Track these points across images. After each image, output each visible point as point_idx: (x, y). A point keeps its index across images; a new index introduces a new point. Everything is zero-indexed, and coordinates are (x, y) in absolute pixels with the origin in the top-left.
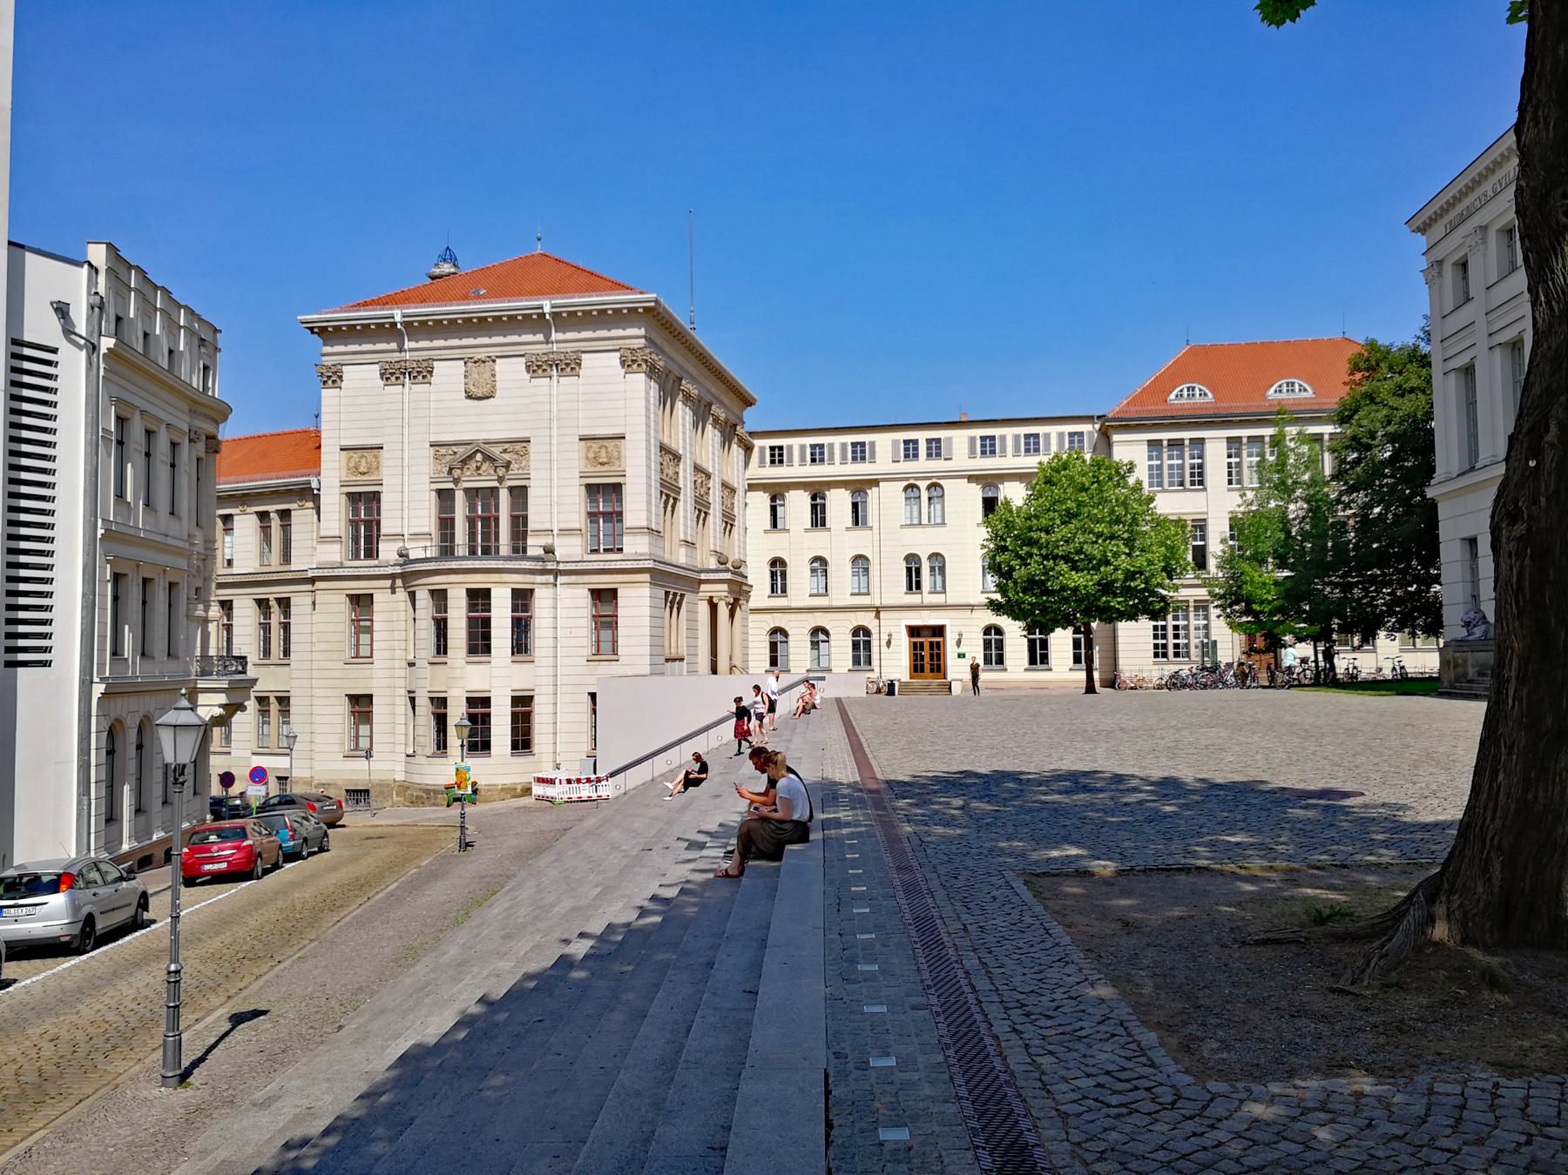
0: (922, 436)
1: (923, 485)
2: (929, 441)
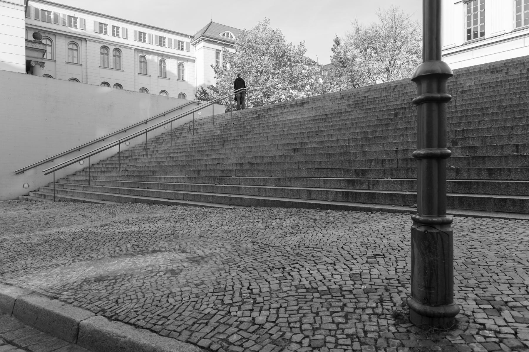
1: (111, 48)
2: (113, 27)
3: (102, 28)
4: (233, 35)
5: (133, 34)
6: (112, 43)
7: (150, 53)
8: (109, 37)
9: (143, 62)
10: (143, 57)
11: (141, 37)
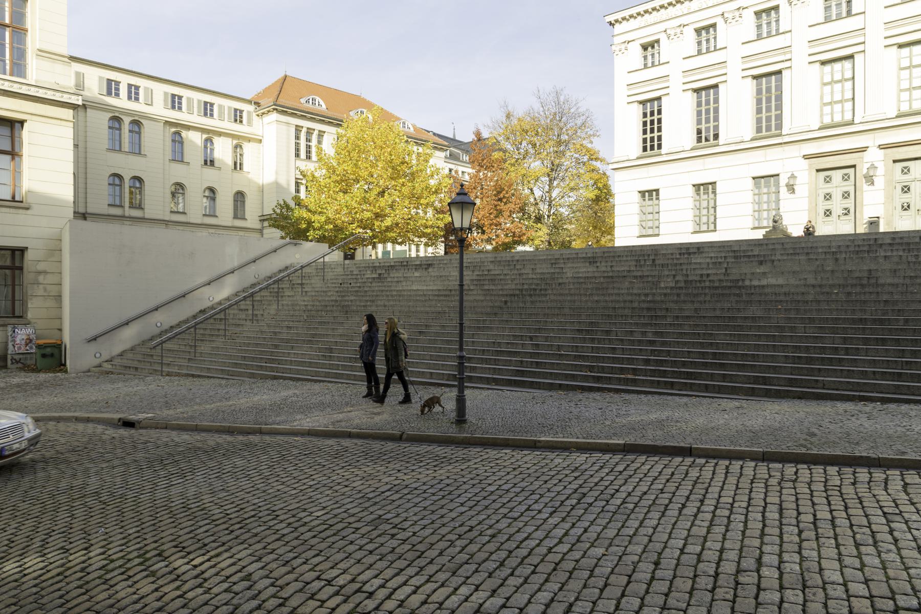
0: (125, 80)
3: (112, 88)
4: (322, 103)
5: (162, 97)
6: (128, 113)
7: (188, 128)
8: (122, 102)
9: (178, 141)
10: (178, 133)
11: (175, 102)
